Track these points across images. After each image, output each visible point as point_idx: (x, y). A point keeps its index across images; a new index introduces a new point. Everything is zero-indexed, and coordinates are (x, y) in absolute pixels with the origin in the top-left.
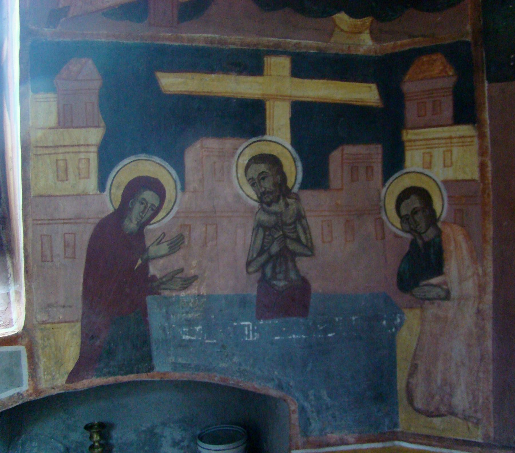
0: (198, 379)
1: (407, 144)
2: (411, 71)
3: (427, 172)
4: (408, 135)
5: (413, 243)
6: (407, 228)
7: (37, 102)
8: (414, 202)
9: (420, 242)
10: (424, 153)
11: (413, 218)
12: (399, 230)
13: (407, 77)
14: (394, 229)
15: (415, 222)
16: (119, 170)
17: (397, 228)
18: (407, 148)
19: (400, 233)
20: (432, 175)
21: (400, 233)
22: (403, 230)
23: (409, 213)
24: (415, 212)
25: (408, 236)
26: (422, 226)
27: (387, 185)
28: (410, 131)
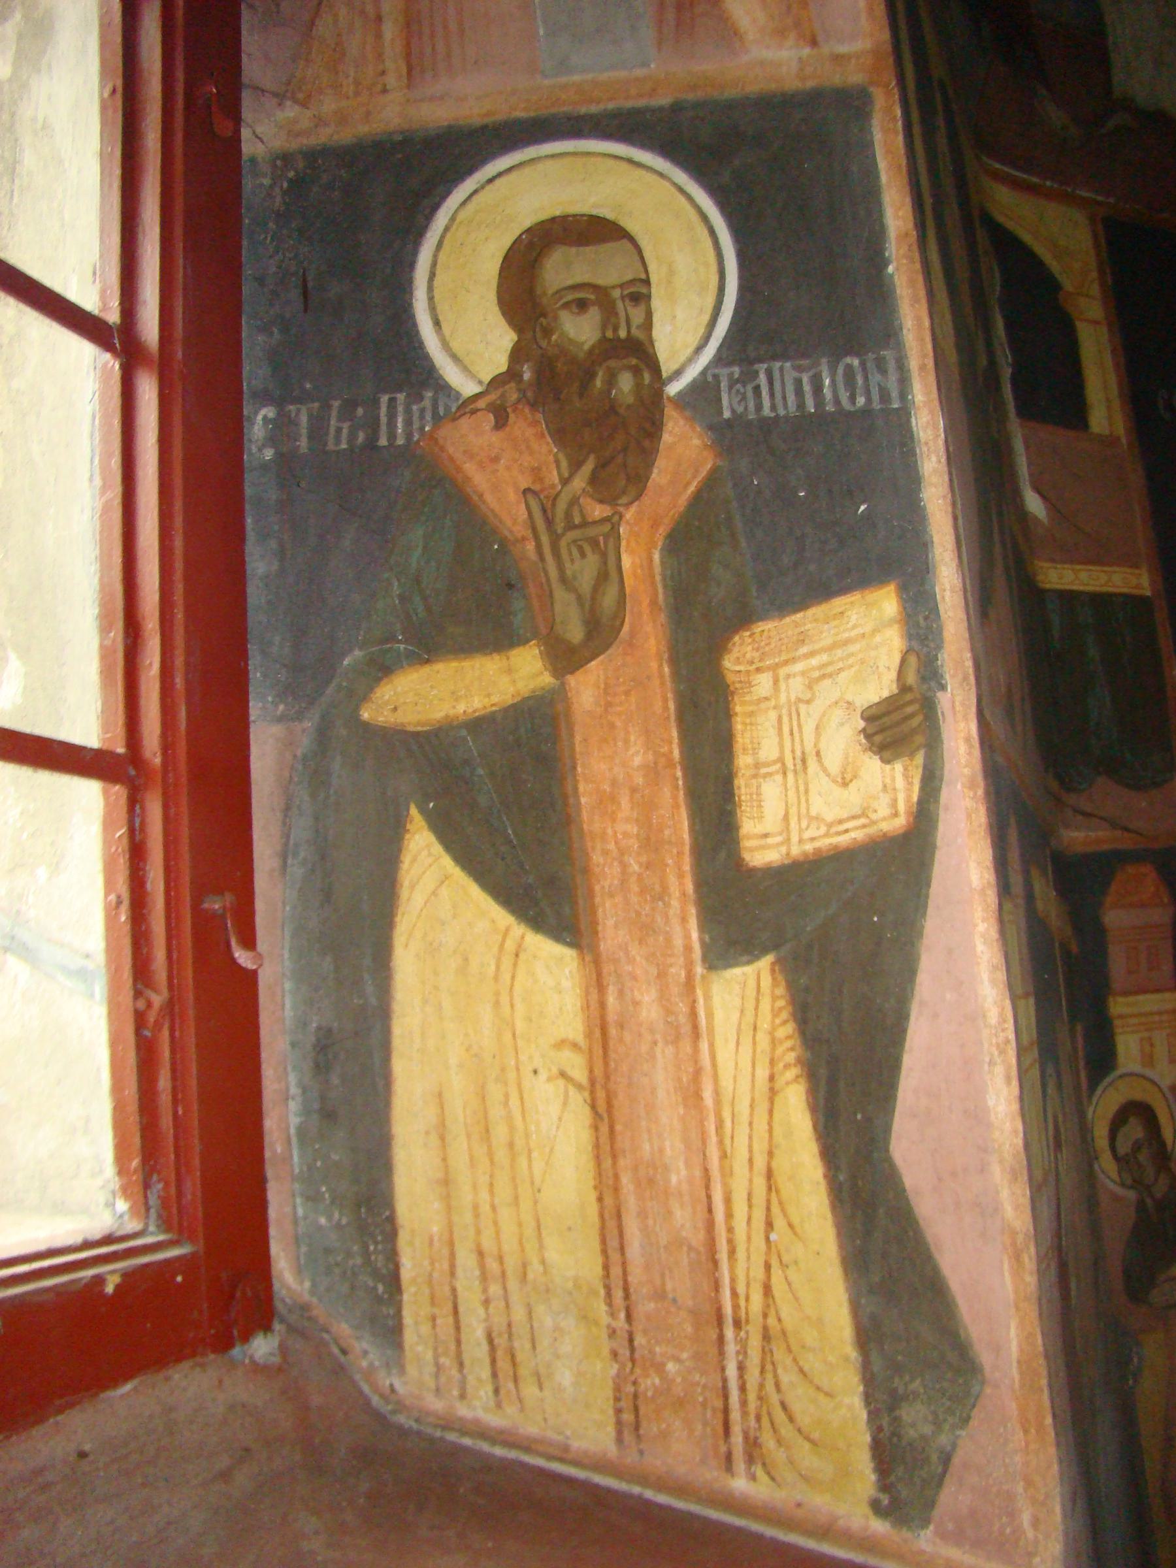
0: (251, 589)
1: (1117, 1022)
2: (1113, 888)
3: (1148, 1072)
4: (1118, 1006)
5: (1141, 1206)
6: (1129, 1182)
7: (864, 814)
8: (1134, 1130)
9: (1149, 1201)
10: (1141, 1040)
11: (1136, 1158)
12: (1115, 1182)
13: (1109, 900)
14: (1111, 1185)
15: (1140, 1166)
16: (500, 175)
17: (1112, 1181)
18: (1118, 1030)
19: (1120, 1191)
20: (1156, 1078)
21: (1120, 1191)
22: (1123, 1185)
23: (1129, 1151)
24: (1137, 1147)
25: (1131, 1195)
26: (1150, 1172)
27: (1095, 1100)
28: (1121, 999)
